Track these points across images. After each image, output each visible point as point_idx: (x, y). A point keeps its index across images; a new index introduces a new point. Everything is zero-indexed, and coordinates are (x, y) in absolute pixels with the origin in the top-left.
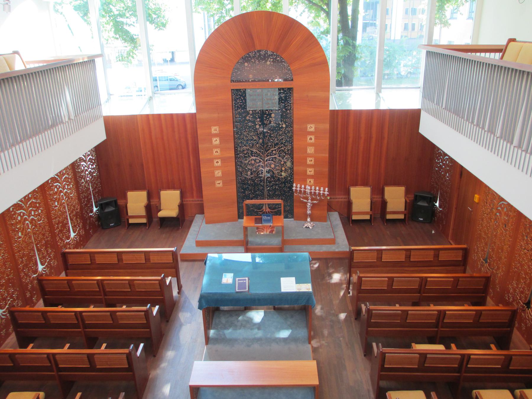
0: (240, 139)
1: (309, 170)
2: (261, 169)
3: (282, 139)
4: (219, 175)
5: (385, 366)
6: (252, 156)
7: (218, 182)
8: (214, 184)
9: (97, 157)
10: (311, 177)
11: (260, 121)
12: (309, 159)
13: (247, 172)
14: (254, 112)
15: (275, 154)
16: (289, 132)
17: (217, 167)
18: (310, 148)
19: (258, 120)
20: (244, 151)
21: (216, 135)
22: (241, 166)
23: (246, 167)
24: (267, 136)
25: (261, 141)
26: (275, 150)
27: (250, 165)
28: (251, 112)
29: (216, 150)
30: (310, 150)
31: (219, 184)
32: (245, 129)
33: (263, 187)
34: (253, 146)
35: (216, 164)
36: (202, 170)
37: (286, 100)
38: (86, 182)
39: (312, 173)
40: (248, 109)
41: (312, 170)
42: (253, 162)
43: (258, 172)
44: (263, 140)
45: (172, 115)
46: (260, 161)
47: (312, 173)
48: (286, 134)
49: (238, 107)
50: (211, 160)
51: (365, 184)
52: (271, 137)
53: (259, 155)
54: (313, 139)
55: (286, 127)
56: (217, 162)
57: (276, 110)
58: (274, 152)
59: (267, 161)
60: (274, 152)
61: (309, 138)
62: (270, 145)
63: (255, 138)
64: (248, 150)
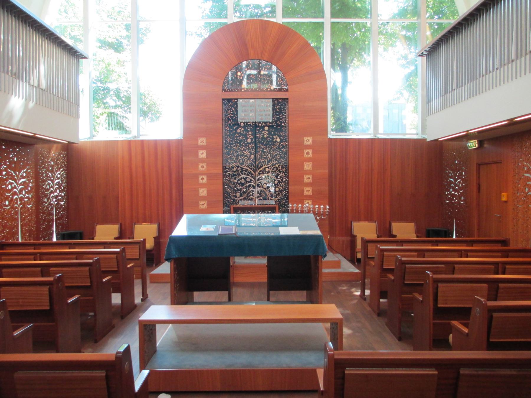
0: (229, 154)
1: (306, 189)
3: (276, 155)
5: (439, 306)
6: (243, 174)
7: (202, 202)
9: (67, 186)
10: (308, 197)
11: (252, 135)
12: (306, 177)
13: (236, 193)
14: (246, 124)
15: (268, 172)
16: (283, 147)
19: (250, 133)
20: (233, 168)
21: (202, 148)
24: (259, 152)
25: (253, 156)
26: (268, 168)
27: (239, 184)
28: (242, 124)
29: (202, 164)
30: (308, 166)
32: (235, 143)
34: (243, 162)
35: (201, 181)
36: (185, 187)
37: (281, 112)
38: (50, 204)
40: (239, 121)
42: (243, 181)
43: (249, 193)
44: (255, 156)
45: (156, 140)
46: (251, 180)
48: (280, 149)
49: (228, 119)
50: (196, 176)
51: (369, 218)
52: (264, 152)
53: (250, 173)
54: (311, 153)
55: (280, 142)
56: (203, 179)
57: (270, 123)
58: (267, 170)
60: (267, 170)
61: (305, 153)
62: (263, 162)
64: (238, 167)
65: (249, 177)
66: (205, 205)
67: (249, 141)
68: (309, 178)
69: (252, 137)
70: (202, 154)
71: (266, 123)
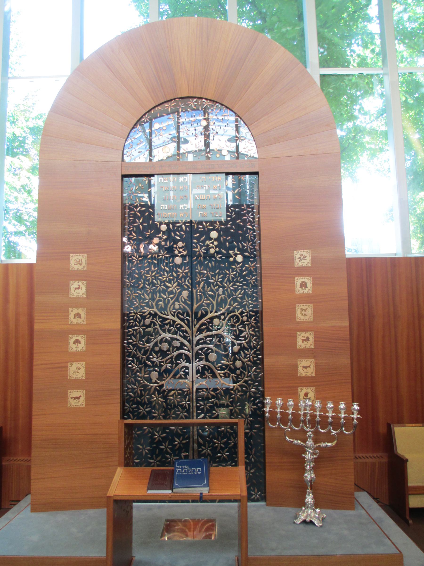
1: (302, 363)
2: (185, 364)
4: (79, 376)
7: (76, 394)
8: (64, 397)
10: (307, 382)
12: (301, 336)
14: (173, 227)
16: (250, 273)
17: (76, 354)
18: (302, 307)
19: (180, 244)
21: (78, 276)
22: (134, 356)
23: (148, 359)
24: (199, 283)
25: (185, 293)
26: (219, 317)
27: (156, 353)
28: (164, 228)
31: (77, 399)
33: (188, 411)
35: (73, 347)
39: (311, 372)
41: (310, 362)
47: (311, 372)
48: (243, 277)
50: (63, 336)
54: (309, 285)
55: (244, 262)
56: (77, 342)
59: (198, 343)
61: (298, 284)
62: (208, 305)
63: (173, 287)
65: (178, 337)
66: (82, 399)
67: (178, 260)
68: (308, 339)
69: (185, 253)
70: (78, 289)
71: (212, 223)
